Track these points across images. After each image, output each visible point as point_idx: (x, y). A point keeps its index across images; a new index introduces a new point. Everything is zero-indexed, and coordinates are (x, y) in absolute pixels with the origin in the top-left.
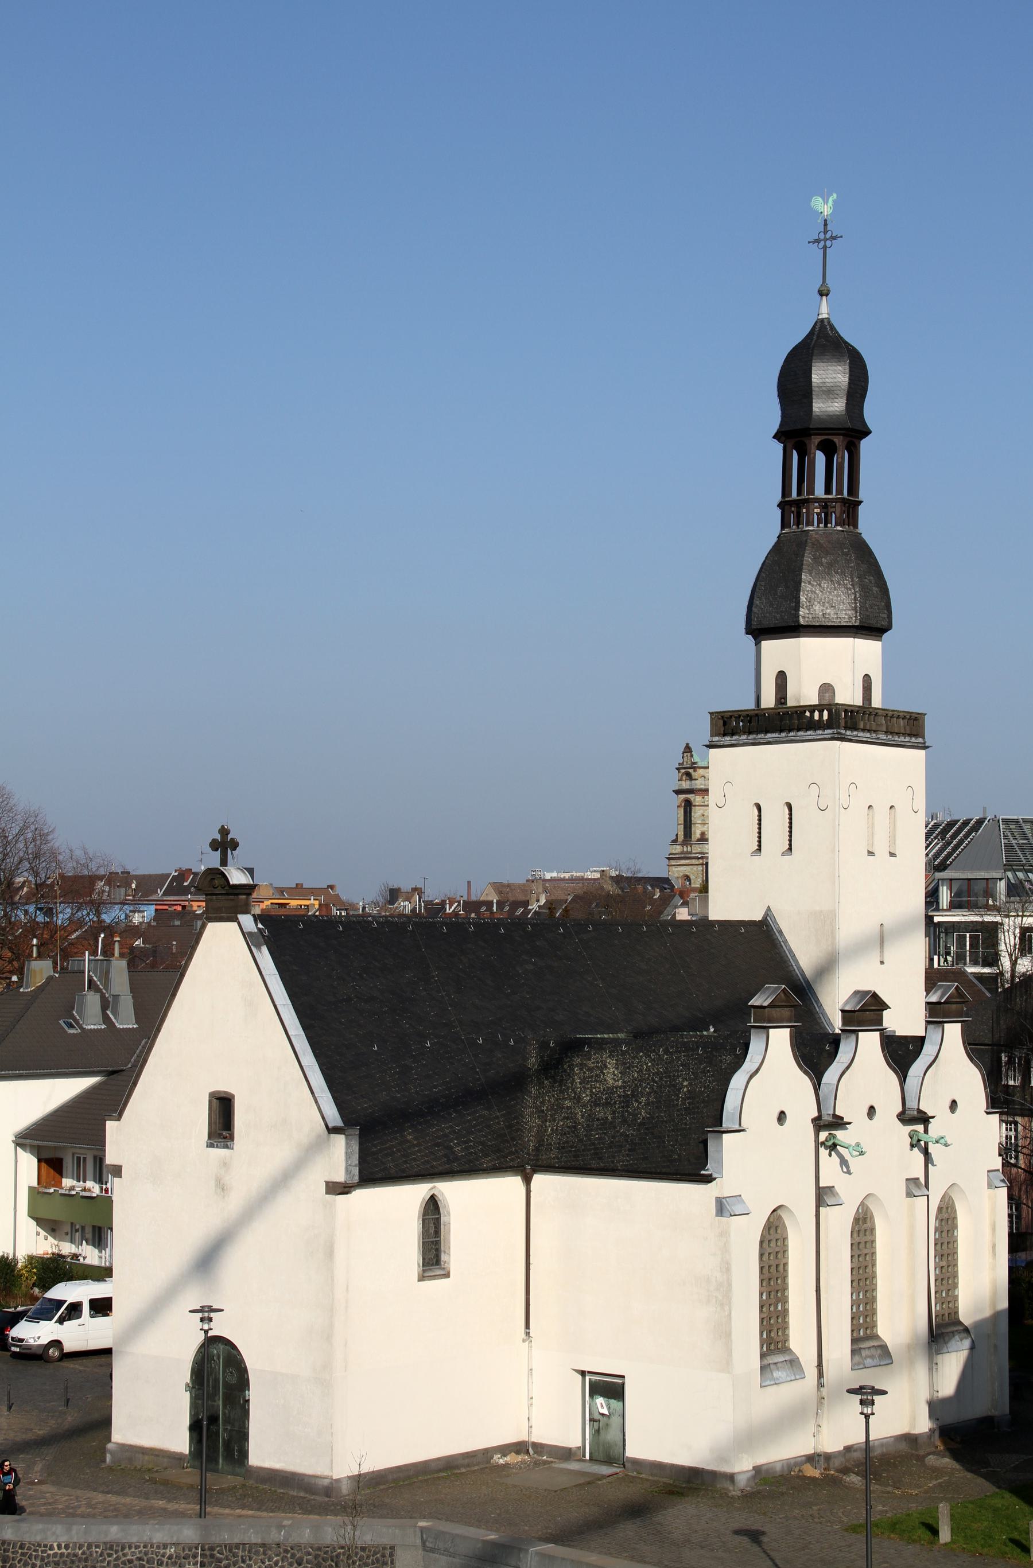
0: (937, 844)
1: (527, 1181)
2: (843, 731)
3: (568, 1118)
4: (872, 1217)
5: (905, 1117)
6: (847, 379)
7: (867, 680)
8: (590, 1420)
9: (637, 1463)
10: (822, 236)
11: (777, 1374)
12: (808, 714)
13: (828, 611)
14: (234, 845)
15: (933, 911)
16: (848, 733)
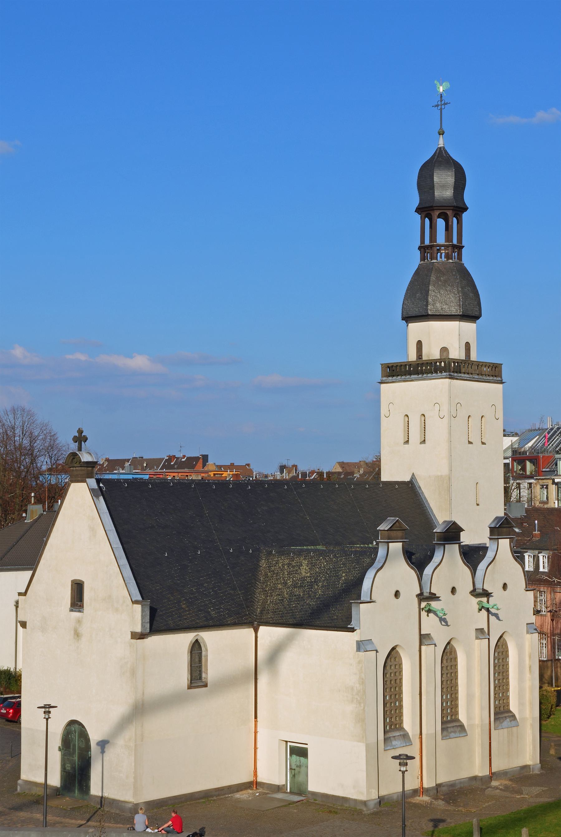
0: (558, 439)
1: (256, 631)
2: (452, 374)
3: (279, 595)
4: (455, 652)
5: (474, 593)
6: (453, 180)
7: (468, 345)
8: (290, 769)
9: (314, 794)
10: (439, 103)
11: (394, 743)
12: (438, 364)
13: (444, 307)
14: (85, 439)
15: (555, 475)
16: (456, 374)
